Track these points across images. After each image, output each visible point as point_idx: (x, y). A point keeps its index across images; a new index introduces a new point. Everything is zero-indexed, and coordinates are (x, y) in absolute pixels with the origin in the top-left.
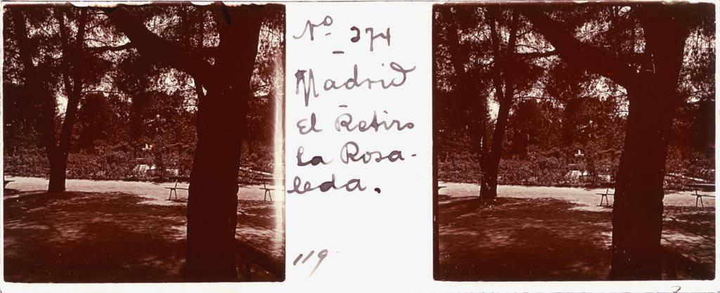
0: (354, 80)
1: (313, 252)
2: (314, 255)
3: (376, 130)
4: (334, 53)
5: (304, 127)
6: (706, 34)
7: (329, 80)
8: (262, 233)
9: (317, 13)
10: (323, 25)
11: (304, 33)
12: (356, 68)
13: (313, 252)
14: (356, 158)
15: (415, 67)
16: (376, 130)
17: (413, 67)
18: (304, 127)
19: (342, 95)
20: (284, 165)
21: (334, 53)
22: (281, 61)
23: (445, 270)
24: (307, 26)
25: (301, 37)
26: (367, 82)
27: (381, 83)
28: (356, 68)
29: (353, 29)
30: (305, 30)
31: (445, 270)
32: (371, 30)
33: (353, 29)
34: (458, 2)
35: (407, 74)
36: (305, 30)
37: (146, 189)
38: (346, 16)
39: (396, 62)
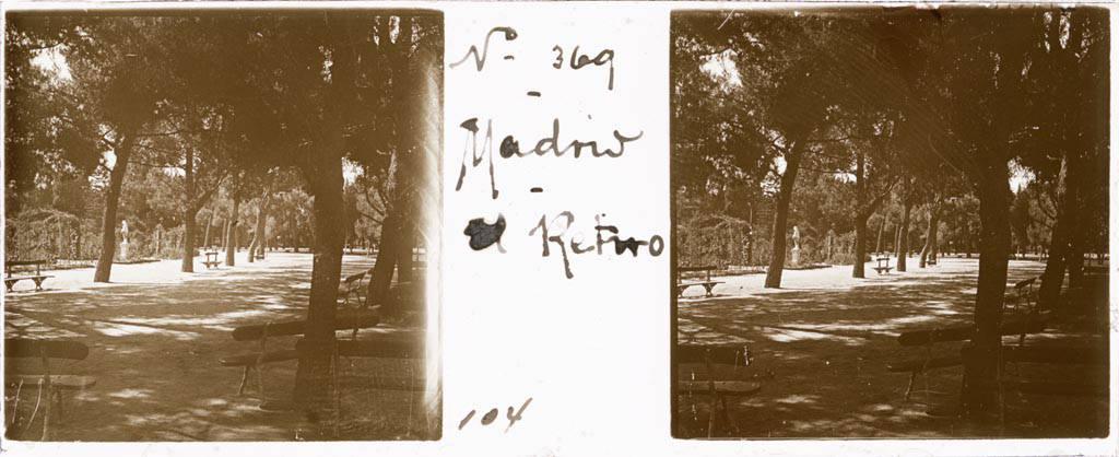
0: (554, 141)
1: (473, 413)
2: (475, 416)
3: (635, 254)
4: (611, 88)
7: (620, 154)
10: (504, 33)
11: (487, 41)
12: (556, 123)
13: (473, 413)
15: (642, 133)
16: (635, 254)
20: (439, 316)
21: (611, 88)
22: (438, 91)
23: (685, 424)
25: (491, 32)
27: (590, 148)
28: (556, 123)
31: (685, 424)
34: (967, 4)
35: (625, 144)
38: (544, 28)
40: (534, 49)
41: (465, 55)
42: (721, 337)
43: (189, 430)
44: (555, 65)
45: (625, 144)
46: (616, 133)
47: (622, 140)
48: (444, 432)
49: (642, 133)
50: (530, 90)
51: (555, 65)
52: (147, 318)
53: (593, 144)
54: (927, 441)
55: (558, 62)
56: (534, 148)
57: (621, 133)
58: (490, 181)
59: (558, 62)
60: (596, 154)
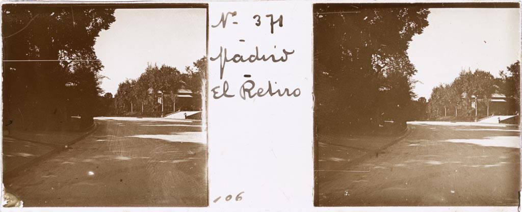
5: (217, 93)
6: (199, 147)
8: (201, 126)
9: (227, 8)
14: (261, 94)
15: (294, 51)
17: (292, 51)
18: (217, 93)
19: (246, 67)
24: (220, 22)
26: (266, 58)
27: (276, 59)
29: (254, 17)
30: (227, 16)
32: (271, 16)
33: (254, 17)
35: (288, 55)
36: (227, 16)
37: (206, 74)
39: (229, 84)
40: (245, 18)
41: (219, 22)
42: (512, 127)
43: (458, 137)
44: (256, 24)
45: (288, 55)
46: (284, 51)
47: (287, 53)
48: (431, 92)
49: (294, 51)
50: (234, 21)
51: (256, 24)
52: (494, 164)
53: (272, 56)
54: (313, 130)
55: (258, 23)
56: (233, 57)
57: (287, 51)
58: (209, 119)
59: (258, 23)
60: (274, 61)
